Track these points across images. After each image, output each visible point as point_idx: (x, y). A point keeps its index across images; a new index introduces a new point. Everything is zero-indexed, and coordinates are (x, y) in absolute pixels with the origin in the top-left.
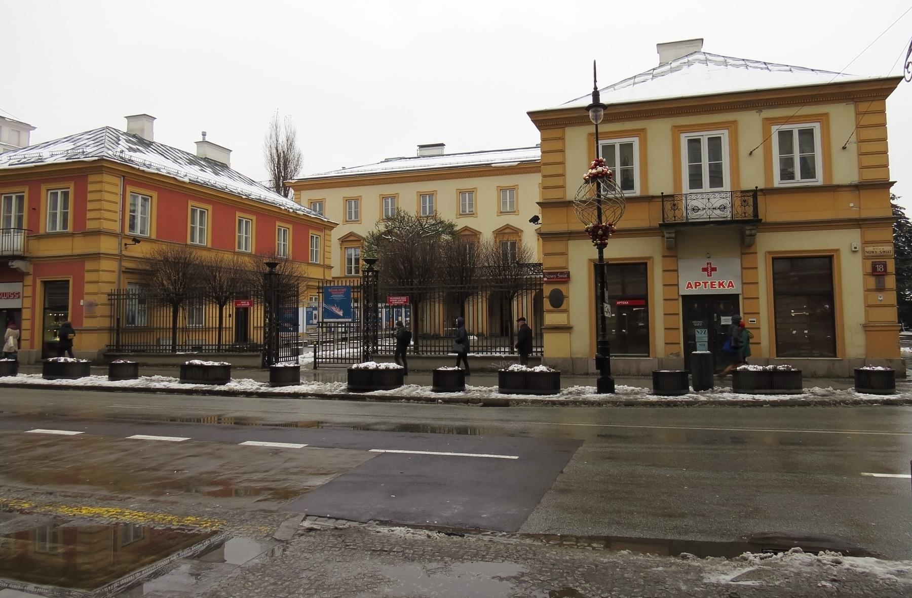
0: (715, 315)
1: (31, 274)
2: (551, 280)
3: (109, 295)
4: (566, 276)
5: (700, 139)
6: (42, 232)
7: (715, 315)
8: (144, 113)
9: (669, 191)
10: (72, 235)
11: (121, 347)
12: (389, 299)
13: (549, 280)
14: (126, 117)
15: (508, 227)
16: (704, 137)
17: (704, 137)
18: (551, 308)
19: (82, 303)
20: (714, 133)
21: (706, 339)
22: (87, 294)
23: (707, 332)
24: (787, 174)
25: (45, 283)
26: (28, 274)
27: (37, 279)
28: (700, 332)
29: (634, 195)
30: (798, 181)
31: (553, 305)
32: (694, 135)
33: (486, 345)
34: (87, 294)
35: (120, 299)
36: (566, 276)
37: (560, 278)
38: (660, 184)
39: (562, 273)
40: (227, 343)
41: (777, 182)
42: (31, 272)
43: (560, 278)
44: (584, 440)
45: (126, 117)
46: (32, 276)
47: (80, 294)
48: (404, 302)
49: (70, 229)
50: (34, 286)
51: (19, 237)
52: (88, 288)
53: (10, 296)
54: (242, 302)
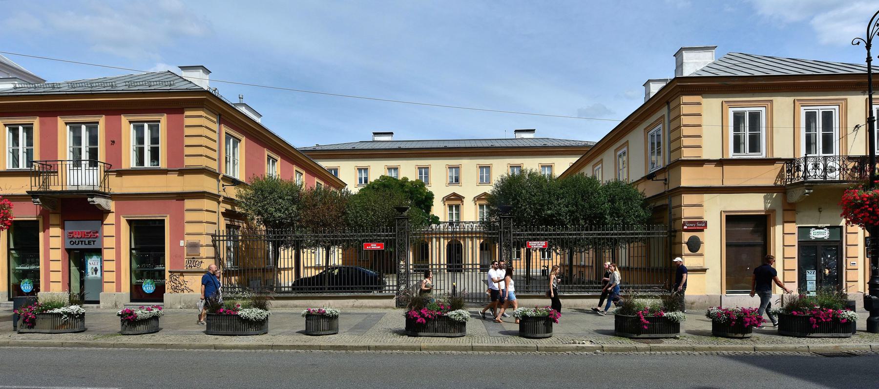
0: (822, 258)
1: (113, 212)
2: (691, 228)
3: (212, 236)
4: (704, 225)
5: (816, 112)
6: (124, 167)
7: (822, 258)
8: (201, 65)
9: (791, 157)
10: (164, 172)
11: (283, 289)
12: (528, 243)
13: (689, 228)
14: (179, 67)
15: (454, 194)
16: (819, 111)
17: (819, 111)
18: (689, 252)
19: (182, 243)
20: (828, 108)
21: (815, 278)
22: (188, 234)
23: (815, 272)
24: (737, 149)
25: (130, 222)
26: (109, 212)
27: (121, 217)
28: (810, 272)
29: (760, 157)
30: (746, 154)
31: (690, 250)
32: (811, 109)
33: (392, 285)
34: (188, 234)
35: (216, 240)
36: (704, 225)
37: (699, 226)
38: (783, 150)
39: (700, 222)
40: (286, 285)
41: (731, 155)
42: (113, 209)
43: (699, 226)
44: (204, 332)
45: (179, 67)
46: (114, 214)
47: (179, 233)
48: (543, 246)
49: (163, 164)
50: (118, 225)
51: (95, 171)
52: (189, 228)
53: (84, 235)
54: (373, 245)
